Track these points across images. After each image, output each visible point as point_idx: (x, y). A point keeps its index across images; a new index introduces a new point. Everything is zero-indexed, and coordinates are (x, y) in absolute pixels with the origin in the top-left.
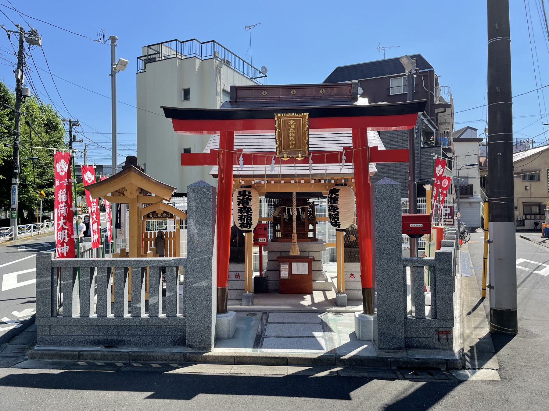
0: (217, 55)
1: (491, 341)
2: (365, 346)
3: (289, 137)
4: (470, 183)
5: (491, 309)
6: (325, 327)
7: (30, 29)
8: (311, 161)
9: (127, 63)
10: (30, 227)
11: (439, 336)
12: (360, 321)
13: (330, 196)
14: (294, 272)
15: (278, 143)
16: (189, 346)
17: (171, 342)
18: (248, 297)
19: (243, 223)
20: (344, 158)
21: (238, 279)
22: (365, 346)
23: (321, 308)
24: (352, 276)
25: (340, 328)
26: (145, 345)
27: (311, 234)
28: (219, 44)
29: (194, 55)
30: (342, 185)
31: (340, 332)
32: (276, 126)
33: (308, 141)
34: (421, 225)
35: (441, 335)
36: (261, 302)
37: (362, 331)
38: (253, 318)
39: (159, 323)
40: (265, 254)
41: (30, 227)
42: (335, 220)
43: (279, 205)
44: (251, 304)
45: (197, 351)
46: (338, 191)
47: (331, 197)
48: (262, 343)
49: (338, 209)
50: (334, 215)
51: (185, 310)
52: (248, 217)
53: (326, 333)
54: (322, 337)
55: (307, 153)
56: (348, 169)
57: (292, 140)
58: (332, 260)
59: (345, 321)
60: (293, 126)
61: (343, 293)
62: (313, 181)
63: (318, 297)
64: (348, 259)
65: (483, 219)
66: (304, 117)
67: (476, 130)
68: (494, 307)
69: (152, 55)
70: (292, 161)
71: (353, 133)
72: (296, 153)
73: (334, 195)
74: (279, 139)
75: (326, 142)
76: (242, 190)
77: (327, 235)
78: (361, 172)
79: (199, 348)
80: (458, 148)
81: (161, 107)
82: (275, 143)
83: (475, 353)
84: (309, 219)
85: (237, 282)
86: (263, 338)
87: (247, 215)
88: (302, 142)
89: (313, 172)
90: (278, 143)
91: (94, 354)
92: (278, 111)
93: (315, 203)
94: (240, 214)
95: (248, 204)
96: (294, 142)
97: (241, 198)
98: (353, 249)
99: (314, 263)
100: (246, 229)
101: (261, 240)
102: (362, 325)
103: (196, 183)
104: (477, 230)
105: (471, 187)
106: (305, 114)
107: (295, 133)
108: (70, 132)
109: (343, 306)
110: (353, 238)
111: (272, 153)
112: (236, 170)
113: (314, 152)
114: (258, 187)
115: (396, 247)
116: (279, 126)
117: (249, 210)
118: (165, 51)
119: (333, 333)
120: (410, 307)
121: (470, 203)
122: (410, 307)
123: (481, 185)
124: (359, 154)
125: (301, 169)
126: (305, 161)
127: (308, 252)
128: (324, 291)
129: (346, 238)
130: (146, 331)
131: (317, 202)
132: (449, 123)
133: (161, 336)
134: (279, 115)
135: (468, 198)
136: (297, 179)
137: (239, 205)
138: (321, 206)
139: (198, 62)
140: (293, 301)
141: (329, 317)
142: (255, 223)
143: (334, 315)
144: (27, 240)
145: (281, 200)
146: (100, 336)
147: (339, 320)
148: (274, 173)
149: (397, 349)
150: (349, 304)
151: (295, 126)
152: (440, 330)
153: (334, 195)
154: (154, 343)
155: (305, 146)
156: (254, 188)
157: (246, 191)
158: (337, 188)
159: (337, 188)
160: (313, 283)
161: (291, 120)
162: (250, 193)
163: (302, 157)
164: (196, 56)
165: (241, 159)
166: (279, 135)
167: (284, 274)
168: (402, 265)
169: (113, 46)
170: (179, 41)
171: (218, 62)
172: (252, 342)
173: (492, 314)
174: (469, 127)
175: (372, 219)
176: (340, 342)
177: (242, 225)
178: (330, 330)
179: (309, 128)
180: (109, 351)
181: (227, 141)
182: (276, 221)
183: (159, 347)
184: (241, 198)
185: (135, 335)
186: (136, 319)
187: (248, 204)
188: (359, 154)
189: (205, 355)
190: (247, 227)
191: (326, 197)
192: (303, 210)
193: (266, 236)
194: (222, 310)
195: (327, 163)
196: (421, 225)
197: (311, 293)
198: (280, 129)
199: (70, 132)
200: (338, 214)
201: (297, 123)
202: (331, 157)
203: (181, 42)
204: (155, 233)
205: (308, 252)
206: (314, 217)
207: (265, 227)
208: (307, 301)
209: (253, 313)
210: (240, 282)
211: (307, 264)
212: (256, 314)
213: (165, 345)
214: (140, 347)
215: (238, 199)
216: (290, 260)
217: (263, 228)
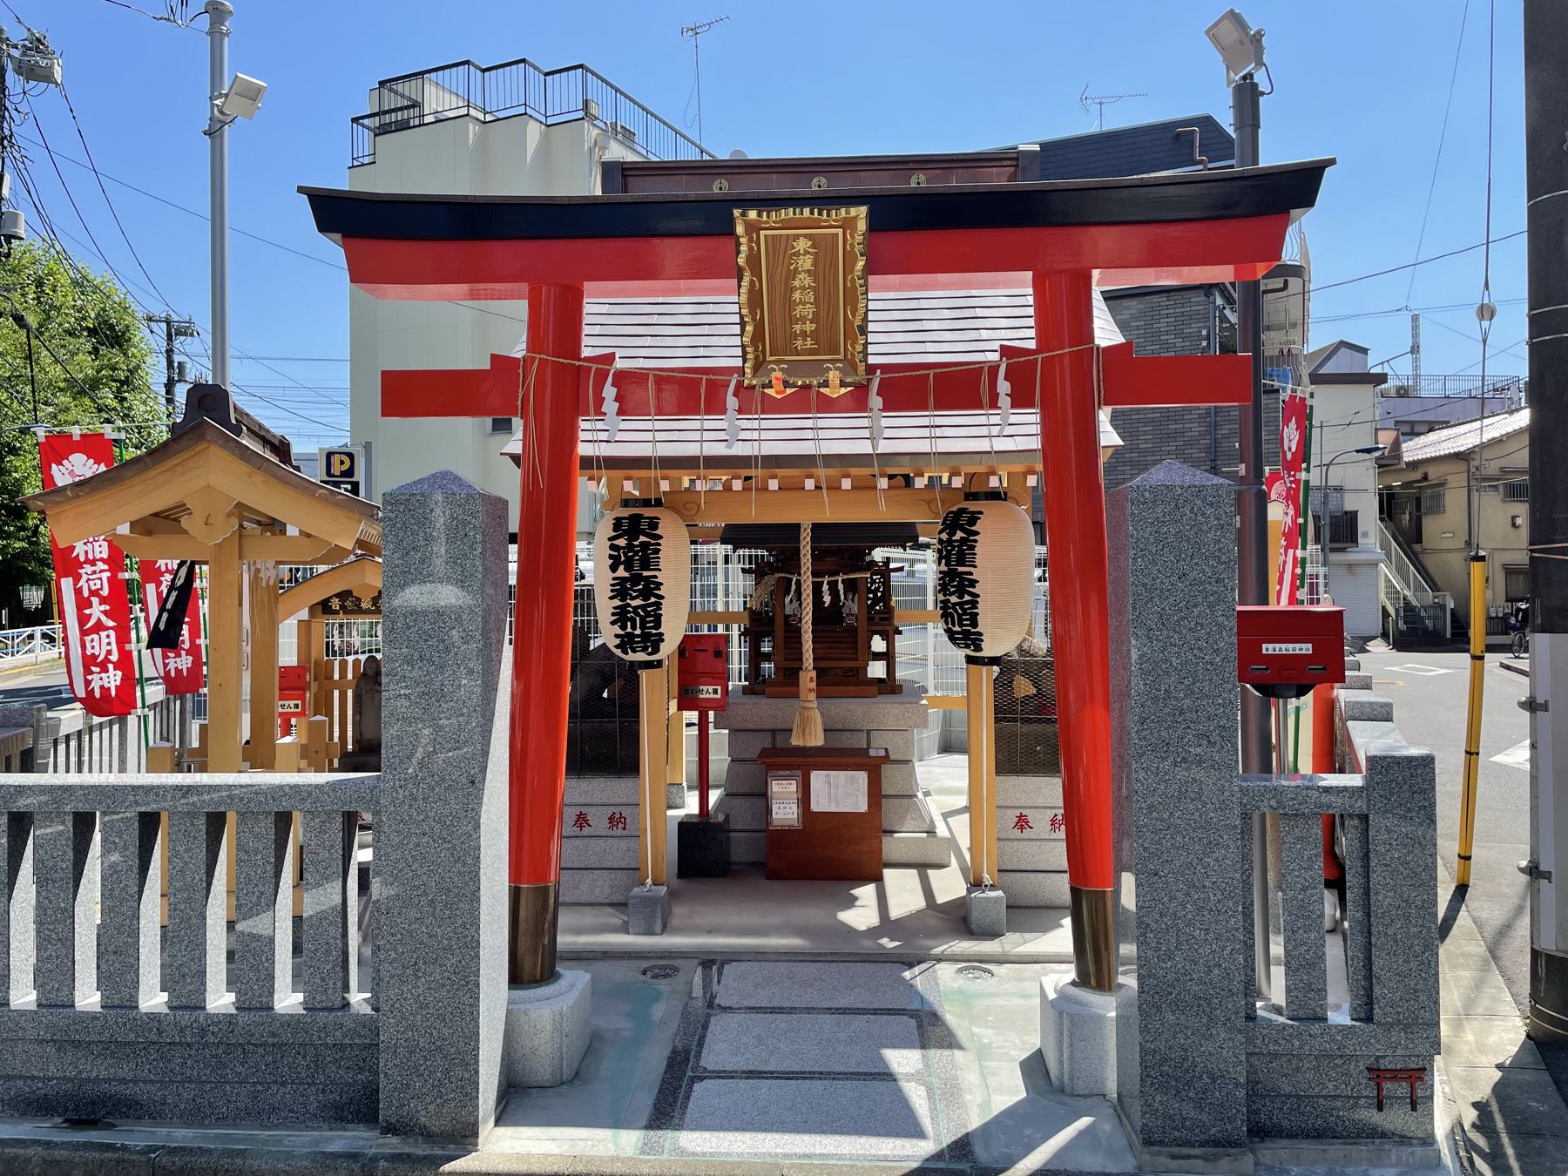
0: (594, 110)
1: (1548, 1078)
2: (1085, 1121)
3: (790, 305)
4: (1348, 508)
5: (1535, 954)
6: (928, 1028)
7: (26, 34)
8: (876, 401)
9: (259, 89)
10: (31, 637)
11: (1379, 1089)
12: (1061, 1013)
13: (944, 536)
14: (819, 804)
15: (749, 328)
16: (390, 1129)
17: (323, 1107)
18: (649, 902)
19: (631, 636)
20: (1004, 387)
21: (619, 832)
22: (1085, 1121)
23: (910, 941)
24: (1022, 822)
25: (986, 1034)
26: (222, 1121)
27: (877, 670)
28: (598, 77)
29: (521, 110)
30: (995, 495)
31: (983, 1053)
32: (741, 260)
33: (865, 320)
34: (1306, 648)
35: (1387, 1086)
36: (699, 920)
37: (1071, 1058)
38: (663, 985)
39: (274, 1035)
40: (719, 737)
41: (31, 637)
42: (962, 625)
43: (772, 568)
44: (658, 927)
45: (421, 1149)
46: (973, 519)
47: (950, 541)
48: (685, 1107)
49: (973, 583)
50: (961, 604)
51: (375, 984)
52: (648, 614)
53: (935, 1054)
54: (916, 1077)
55: (862, 367)
56: (1015, 432)
57: (803, 319)
58: (947, 747)
59: (1001, 1002)
60: (806, 263)
61: (993, 887)
62: (883, 483)
63: (903, 893)
64: (1012, 761)
65: (1385, 614)
66: (847, 225)
67: (1364, 351)
68: (1549, 944)
69: (401, 109)
70: (806, 401)
71: (1037, 284)
72: (818, 368)
73: (959, 535)
74: (752, 313)
75: (930, 347)
76: (626, 512)
77: (931, 668)
78: (1068, 443)
79: (428, 1136)
80: (1326, 404)
81: (301, 190)
82: (737, 329)
83: (1505, 1139)
84: (870, 619)
85: (616, 841)
86: (693, 1080)
87: (643, 607)
88: (841, 330)
89: (884, 447)
90: (749, 328)
91: (16, 1157)
92: (746, 203)
93: (892, 566)
94: (617, 602)
95: (646, 565)
96: (809, 327)
97: (622, 542)
98: (1033, 724)
99: (886, 770)
100: (641, 656)
101: (708, 692)
102: (1072, 1035)
103: (421, 481)
104: (1371, 646)
105: (1352, 517)
106: (853, 211)
107: (816, 290)
108: (169, 352)
109: (992, 934)
110: (1023, 687)
111: (729, 371)
112: (592, 438)
113: (886, 368)
114: (682, 503)
115: (1215, 737)
116: (754, 259)
117: (651, 589)
118: (436, 99)
119: (956, 1052)
120: (1276, 987)
121: (1350, 566)
122: (1276, 987)
123: (1381, 512)
124: (1053, 375)
125: (839, 435)
126: (857, 401)
127: (869, 732)
128: (922, 867)
129: (1003, 686)
130: (224, 1066)
131: (896, 560)
132: (1294, 325)
133: (283, 1084)
134: (753, 214)
135: (1343, 550)
136: (822, 472)
137: (614, 568)
138: (911, 574)
139: (534, 131)
140: (809, 913)
141: (942, 982)
142: (673, 630)
143: (960, 971)
144: (20, 675)
145: (773, 549)
146: (58, 1069)
147: (979, 996)
148: (739, 450)
149: (1216, 1143)
150: (1013, 927)
151: (815, 264)
152: (1384, 1064)
153: (959, 535)
154: (257, 1114)
155: (855, 342)
156: (674, 509)
157: (640, 516)
158: (972, 506)
159: (972, 506)
160: (886, 840)
161: (799, 240)
162: (654, 524)
163: (843, 384)
164: (529, 111)
165: (609, 392)
166: (755, 299)
167: (785, 812)
168: (1237, 810)
169: (216, 34)
170: (477, 67)
171: (596, 131)
172: (645, 1101)
173: (1542, 971)
174: (1343, 344)
175: (1112, 622)
176: (986, 1104)
177: (626, 643)
178: (949, 1041)
179: (871, 269)
180: (78, 1146)
181: (558, 324)
182: (759, 624)
183: (276, 1127)
184: (622, 542)
185: (182, 1082)
186: (185, 1017)
187: (646, 565)
188: (1053, 375)
189: (447, 1168)
190: (644, 649)
191: (927, 546)
192: (851, 586)
193: (722, 677)
194: (532, 965)
195: (936, 409)
196: (1306, 648)
197: (878, 879)
198: (756, 272)
199: (169, 352)
200: (974, 604)
201: (824, 249)
202: (956, 387)
203: (484, 71)
204: (356, 662)
205: (869, 732)
206: (889, 610)
207: (719, 649)
208: (861, 913)
209: (663, 965)
210: (623, 844)
211: (862, 777)
212: (676, 970)
213: (301, 1119)
214: (201, 1125)
215: (612, 547)
216: (802, 762)
217: (711, 651)
